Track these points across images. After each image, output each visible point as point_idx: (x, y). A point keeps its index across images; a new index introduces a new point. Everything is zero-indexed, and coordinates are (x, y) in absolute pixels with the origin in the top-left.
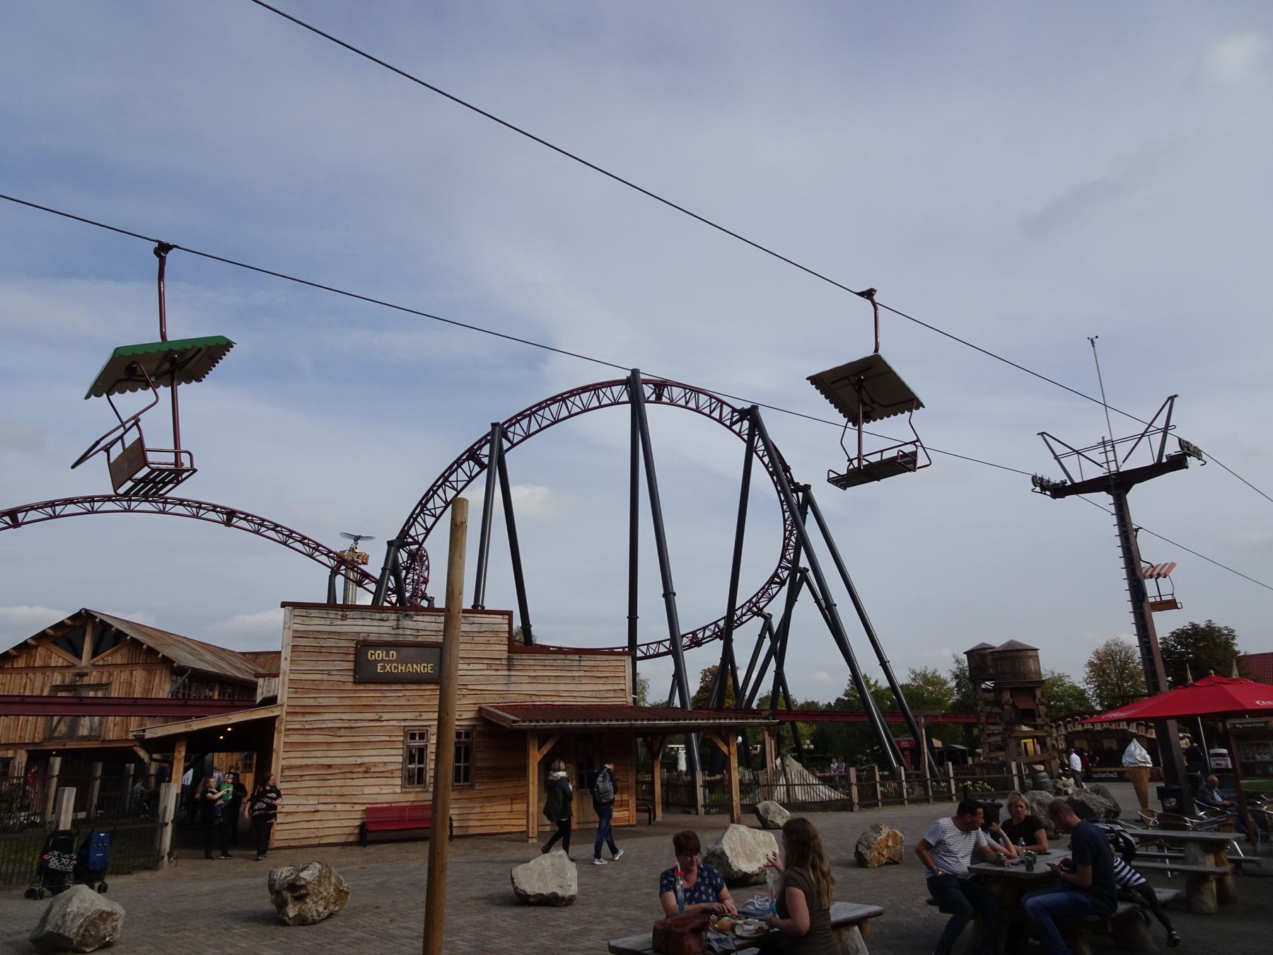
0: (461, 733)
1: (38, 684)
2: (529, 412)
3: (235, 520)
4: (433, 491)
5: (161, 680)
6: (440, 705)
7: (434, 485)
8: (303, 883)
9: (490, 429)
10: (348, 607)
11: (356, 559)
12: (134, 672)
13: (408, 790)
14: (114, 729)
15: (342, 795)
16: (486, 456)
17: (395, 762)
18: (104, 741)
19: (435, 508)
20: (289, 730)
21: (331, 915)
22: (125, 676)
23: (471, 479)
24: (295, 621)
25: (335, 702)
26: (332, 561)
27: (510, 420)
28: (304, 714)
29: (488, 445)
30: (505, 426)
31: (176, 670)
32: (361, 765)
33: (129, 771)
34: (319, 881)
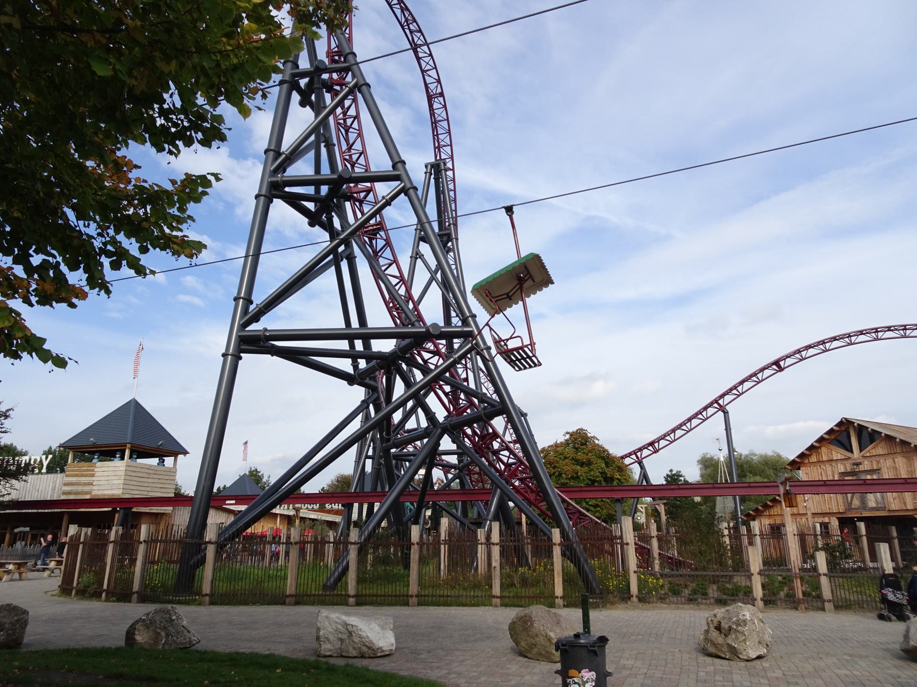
1: (829, 473)
12: (896, 460)
18: (889, 511)
22: (889, 462)
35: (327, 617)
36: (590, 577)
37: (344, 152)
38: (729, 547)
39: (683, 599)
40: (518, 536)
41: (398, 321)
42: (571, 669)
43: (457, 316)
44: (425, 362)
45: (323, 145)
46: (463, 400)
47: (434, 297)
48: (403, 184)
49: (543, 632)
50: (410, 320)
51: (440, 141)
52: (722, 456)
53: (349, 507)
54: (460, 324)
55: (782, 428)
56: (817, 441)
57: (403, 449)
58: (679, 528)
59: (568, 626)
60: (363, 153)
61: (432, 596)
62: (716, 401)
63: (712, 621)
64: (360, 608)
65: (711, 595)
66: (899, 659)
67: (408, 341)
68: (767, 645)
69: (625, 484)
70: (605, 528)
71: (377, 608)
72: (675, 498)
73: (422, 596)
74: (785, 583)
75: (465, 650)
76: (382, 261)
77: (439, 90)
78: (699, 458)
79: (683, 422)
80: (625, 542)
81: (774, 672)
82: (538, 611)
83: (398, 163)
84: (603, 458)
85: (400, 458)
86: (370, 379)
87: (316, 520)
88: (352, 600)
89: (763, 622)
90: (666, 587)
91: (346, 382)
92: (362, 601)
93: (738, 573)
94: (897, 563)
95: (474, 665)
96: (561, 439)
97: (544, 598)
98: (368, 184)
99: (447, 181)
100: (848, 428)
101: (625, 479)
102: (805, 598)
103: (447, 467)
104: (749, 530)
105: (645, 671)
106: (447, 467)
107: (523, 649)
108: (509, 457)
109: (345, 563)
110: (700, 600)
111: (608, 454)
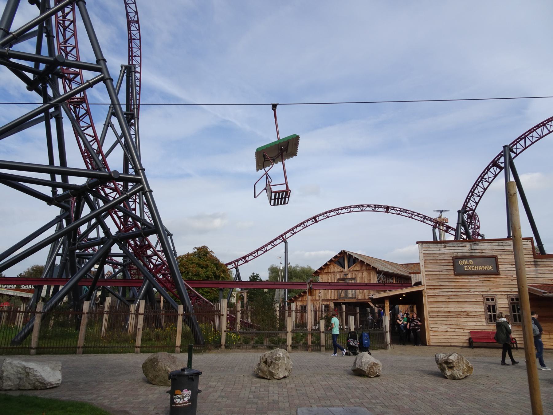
0: (513, 298)
1: (333, 279)
2: (524, 136)
3: (389, 210)
4: (476, 185)
5: (373, 276)
6: (518, 284)
7: (476, 182)
8: (451, 361)
9: (502, 149)
10: (442, 242)
11: (442, 221)
12: (363, 273)
13: (490, 324)
14: (362, 295)
15: (457, 325)
16: (503, 163)
17: (481, 311)
18: (357, 299)
19: (479, 193)
20: (429, 296)
21: (466, 377)
22: (360, 274)
23: (496, 175)
24: (424, 249)
25: (447, 284)
26: (433, 223)
27: (514, 142)
28: (434, 289)
29: (503, 158)
30: (511, 146)
31: (379, 272)
32: (464, 312)
33: (368, 311)
34: (458, 361)
35: (10, 363)
36: (199, 334)
37: (61, 44)
38: (278, 317)
39: (250, 346)
40: (157, 309)
41: (90, 167)
42: (176, 390)
43: (133, 168)
44: (107, 195)
45: (44, 35)
46: (131, 222)
47: (119, 152)
48: (103, 75)
49: (164, 368)
50: (98, 166)
51: (133, 52)
52: (281, 267)
53: (40, 288)
54: (134, 173)
55: (313, 253)
56: (329, 261)
57: (85, 251)
58: (253, 306)
59: (180, 364)
60: (76, 47)
61: (94, 347)
62: (282, 236)
63: (263, 358)
64: (39, 356)
65: (265, 344)
66: (350, 375)
67: (95, 180)
68: (289, 371)
69: (227, 280)
70: (211, 305)
71: (52, 356)
72: (254, 289)
73: (86, 347)
74: (304, 337)
75: (111, 381)
76: (82, 124)
77: (136, 19)
78: (269, 267)
79: (263, 246)
80: (221, 314)
81: (291, 385)
82: (162, 356)
83: (101, 60)
84: (216, 264)
85: (82, 257)
86: (65, 202)
87: (13, 296)
88: (33, 351)
89: (289, 358)
90: (242, 340)
91: (46, 203)
92: (40, 351)
93: (281, 332)
94: (357, 327)
95: (116, 391)
96: (192, 251)
97: (169, 347)
98: (77, 70)
99: (135, 80)
100: (344, 255)
101: (227, 277)
102: (312, 344)
103: (115, 265)
104: (290, 308)
105: (222, 388)
106: (115, 265)
107: (150, 379)
108: (157, 260)
109: (30, 326)
110: (259, 347)
111: (219, 262)
